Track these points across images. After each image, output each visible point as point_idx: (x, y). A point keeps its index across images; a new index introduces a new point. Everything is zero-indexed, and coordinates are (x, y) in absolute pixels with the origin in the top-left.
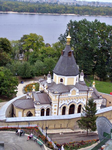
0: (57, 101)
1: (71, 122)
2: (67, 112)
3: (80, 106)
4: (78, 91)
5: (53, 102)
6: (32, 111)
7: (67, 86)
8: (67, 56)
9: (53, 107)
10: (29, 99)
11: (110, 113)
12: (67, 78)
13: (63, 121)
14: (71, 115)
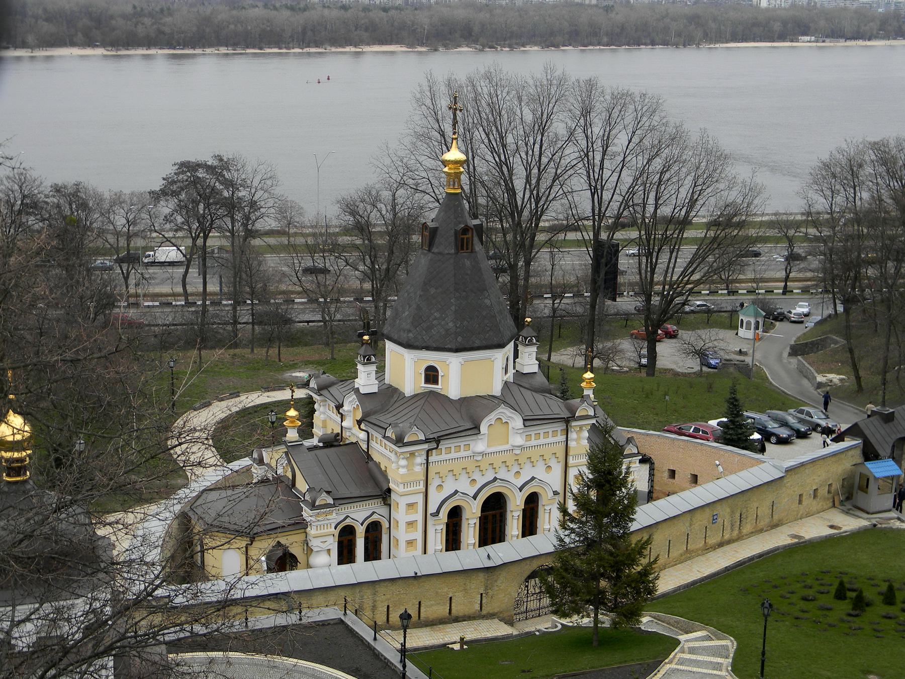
0: (417, 482)
1: (499, 582)
2: (470, 533)
3: (532, 501)
4: (517, 422)
5: (398, 486)
6: (292, 542)
7: (464, 401)
8: (453, 251)
9: (401, 515)
10: (268, 480)
11: (687, 524)
12: (460, 359)
13: (460, 580)
14: (489, 549)
